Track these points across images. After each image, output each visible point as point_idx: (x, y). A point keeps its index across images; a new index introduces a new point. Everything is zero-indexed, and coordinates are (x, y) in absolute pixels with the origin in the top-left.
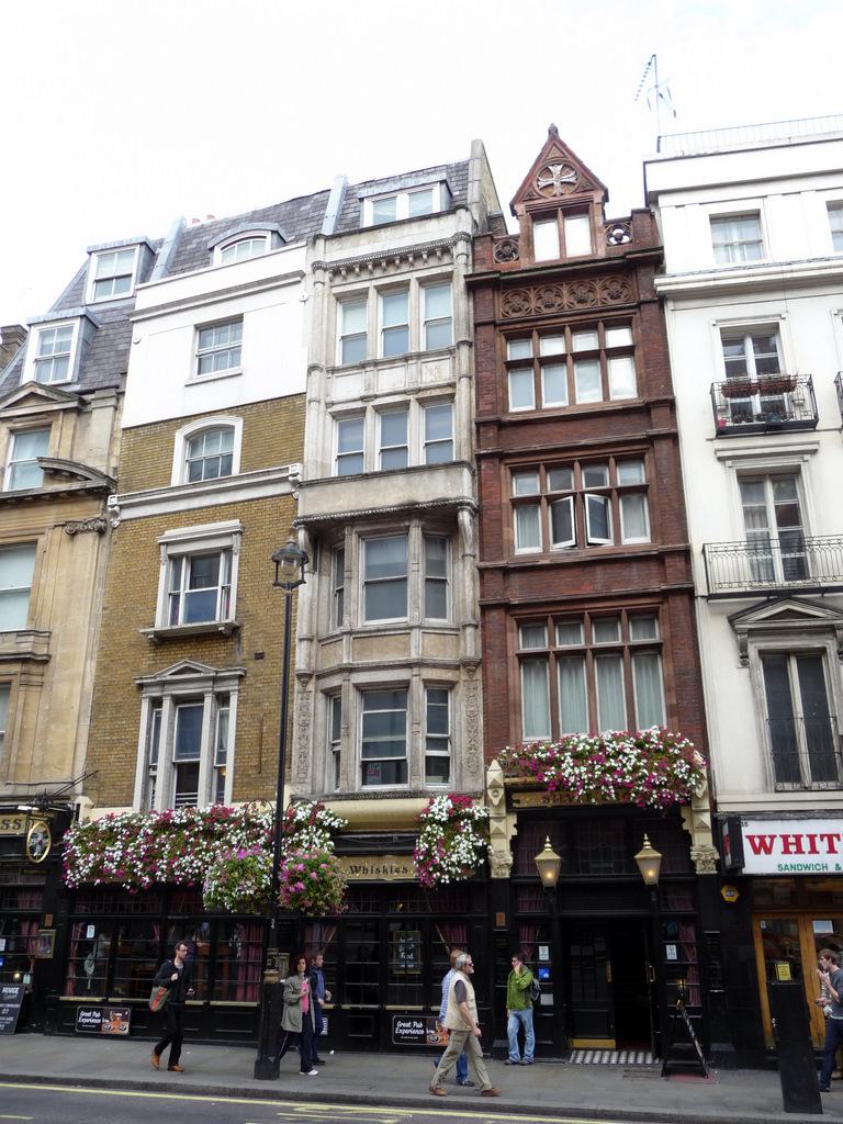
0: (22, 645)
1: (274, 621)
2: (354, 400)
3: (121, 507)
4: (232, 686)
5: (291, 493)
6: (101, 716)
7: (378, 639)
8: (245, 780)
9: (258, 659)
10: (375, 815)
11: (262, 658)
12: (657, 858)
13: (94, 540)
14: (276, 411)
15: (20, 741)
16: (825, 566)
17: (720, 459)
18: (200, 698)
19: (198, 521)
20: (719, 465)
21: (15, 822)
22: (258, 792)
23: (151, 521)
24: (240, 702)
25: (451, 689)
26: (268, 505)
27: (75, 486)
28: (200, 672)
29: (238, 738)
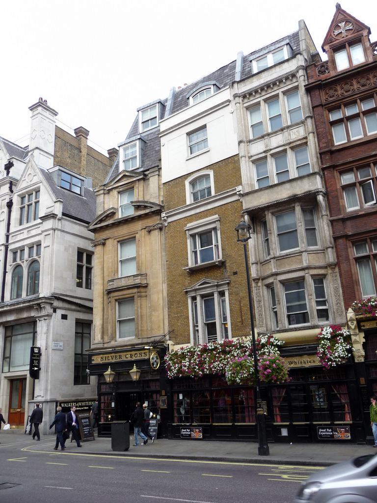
0: (136, 281)
3: (167, 217)
4: (225, 288)
5: (239, 200)
8: (237, 328)
18: (212, 294)
19: (201, 218)
23: (181, 221)
26: (229, 206)
27: (147, 211)
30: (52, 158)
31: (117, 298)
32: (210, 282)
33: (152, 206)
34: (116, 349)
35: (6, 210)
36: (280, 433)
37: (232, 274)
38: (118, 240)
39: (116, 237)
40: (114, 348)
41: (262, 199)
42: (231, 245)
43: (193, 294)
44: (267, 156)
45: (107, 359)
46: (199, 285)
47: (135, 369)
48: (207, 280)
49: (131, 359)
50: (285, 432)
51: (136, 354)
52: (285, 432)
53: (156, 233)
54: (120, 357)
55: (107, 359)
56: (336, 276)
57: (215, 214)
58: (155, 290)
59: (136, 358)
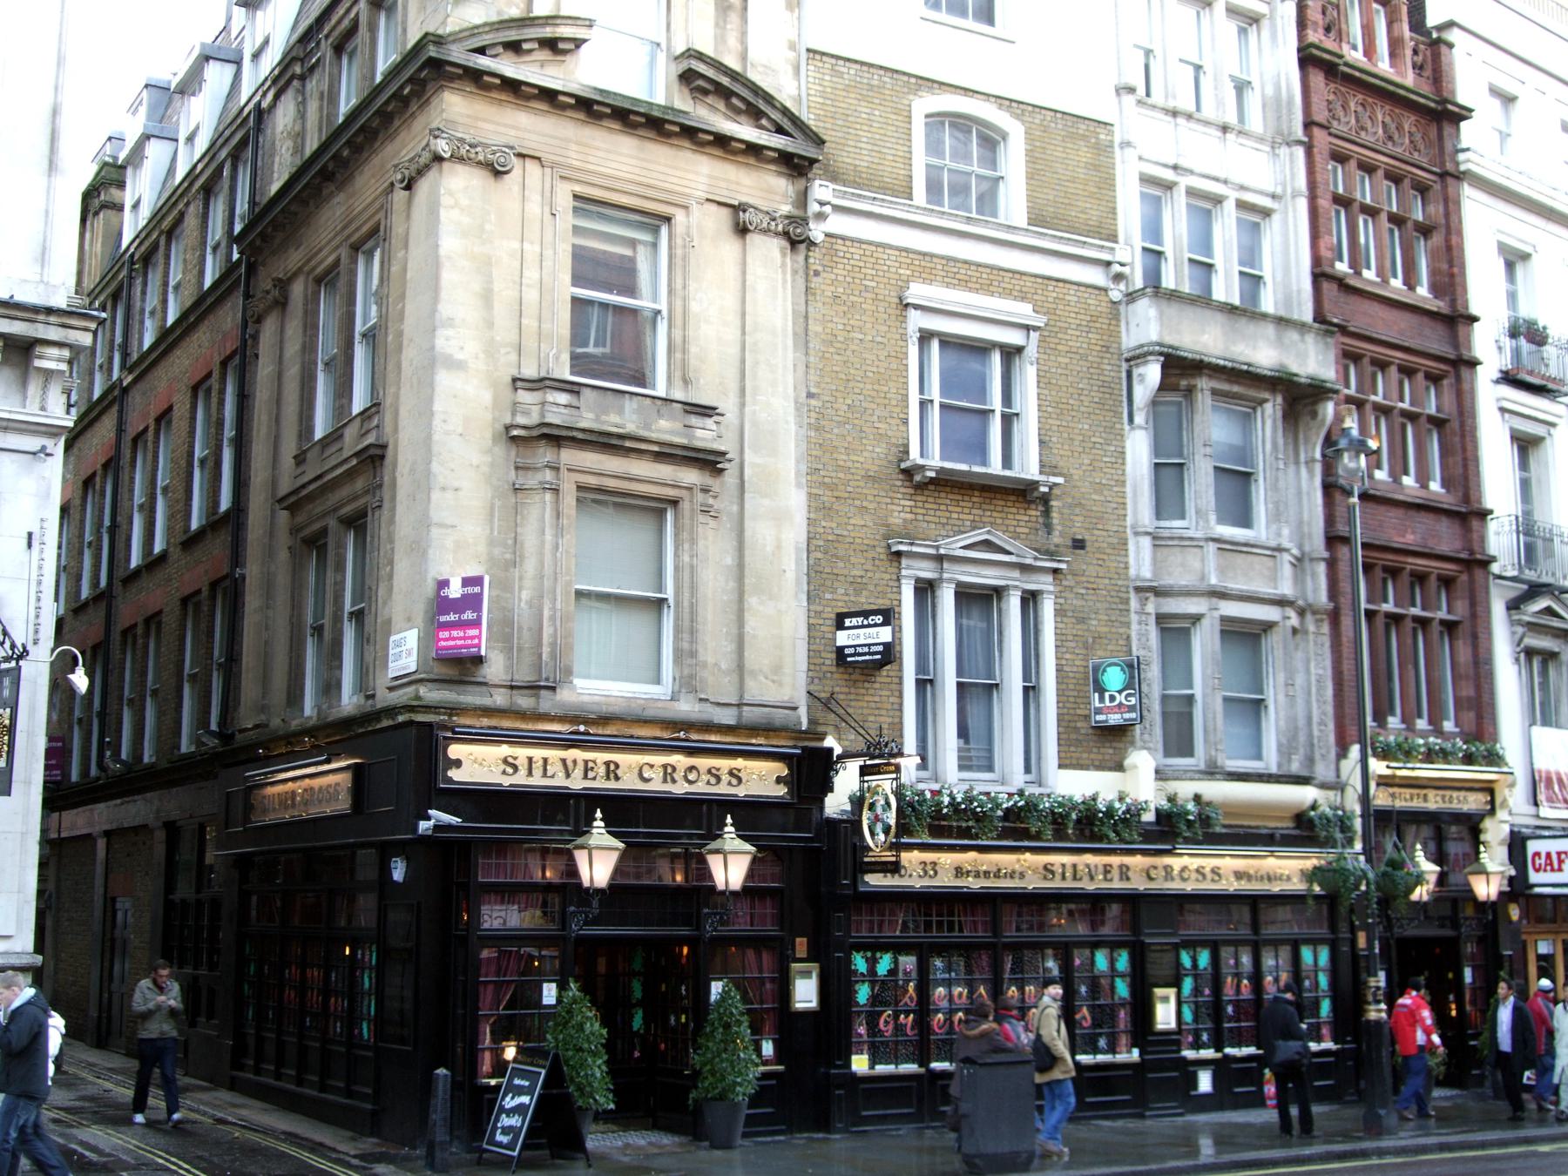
0: (699, 433)
1: (1096, 492)
2: (1166, 166)
3: (837, 208)
4: (1044, 583)
5: (1105, 290)
6: (828, 596)
7: (1243, 555)
8: (1073, 736)
9: (1075, 547)
10: (192, 714)
11: (1075, 541)
12: (748, 853)
13: (784, 255)
14: (1073, 137)
15: (542, 577)
16: (637, 171)
17: (1503, 410)
18: (998, 592)
19: (965, 284)
20: (1498, 414)
21: (731, 773)
22: (1092, 756)
23: (880, 253)
24: (1059, 612)
25: (1265, 631)
26: (1072, 295)
27: (746, 132)
28: (1009, 553)
29: (1060, 668)
30: (1467, 162)
31: (592, 481)
32: (1008, 547)
33: (787, 124)
34: (694, 736)
35: (1171, 162)
36: (1194, 1082)
37: (1070, 543)
38: (578, 189)
39: (570, 167)
40: (586, 722)
41: (1206, 336)
42: (1072, 439)
43: (927, 571)
44: (1175, 184)
45: (537, 772)
46: (963, 548)
47: (599, 833)
48: (999, 538)
49: (668, 787)
50: (1205, 1082)
51: (692, 768)
52: (1205, 1082)
53: (767, 251)
54: (1425, 798)
55: (537, 772)
56: (1322, 645)
57: (1023, 299)
58: (766, 502)
59: (692, 789)
